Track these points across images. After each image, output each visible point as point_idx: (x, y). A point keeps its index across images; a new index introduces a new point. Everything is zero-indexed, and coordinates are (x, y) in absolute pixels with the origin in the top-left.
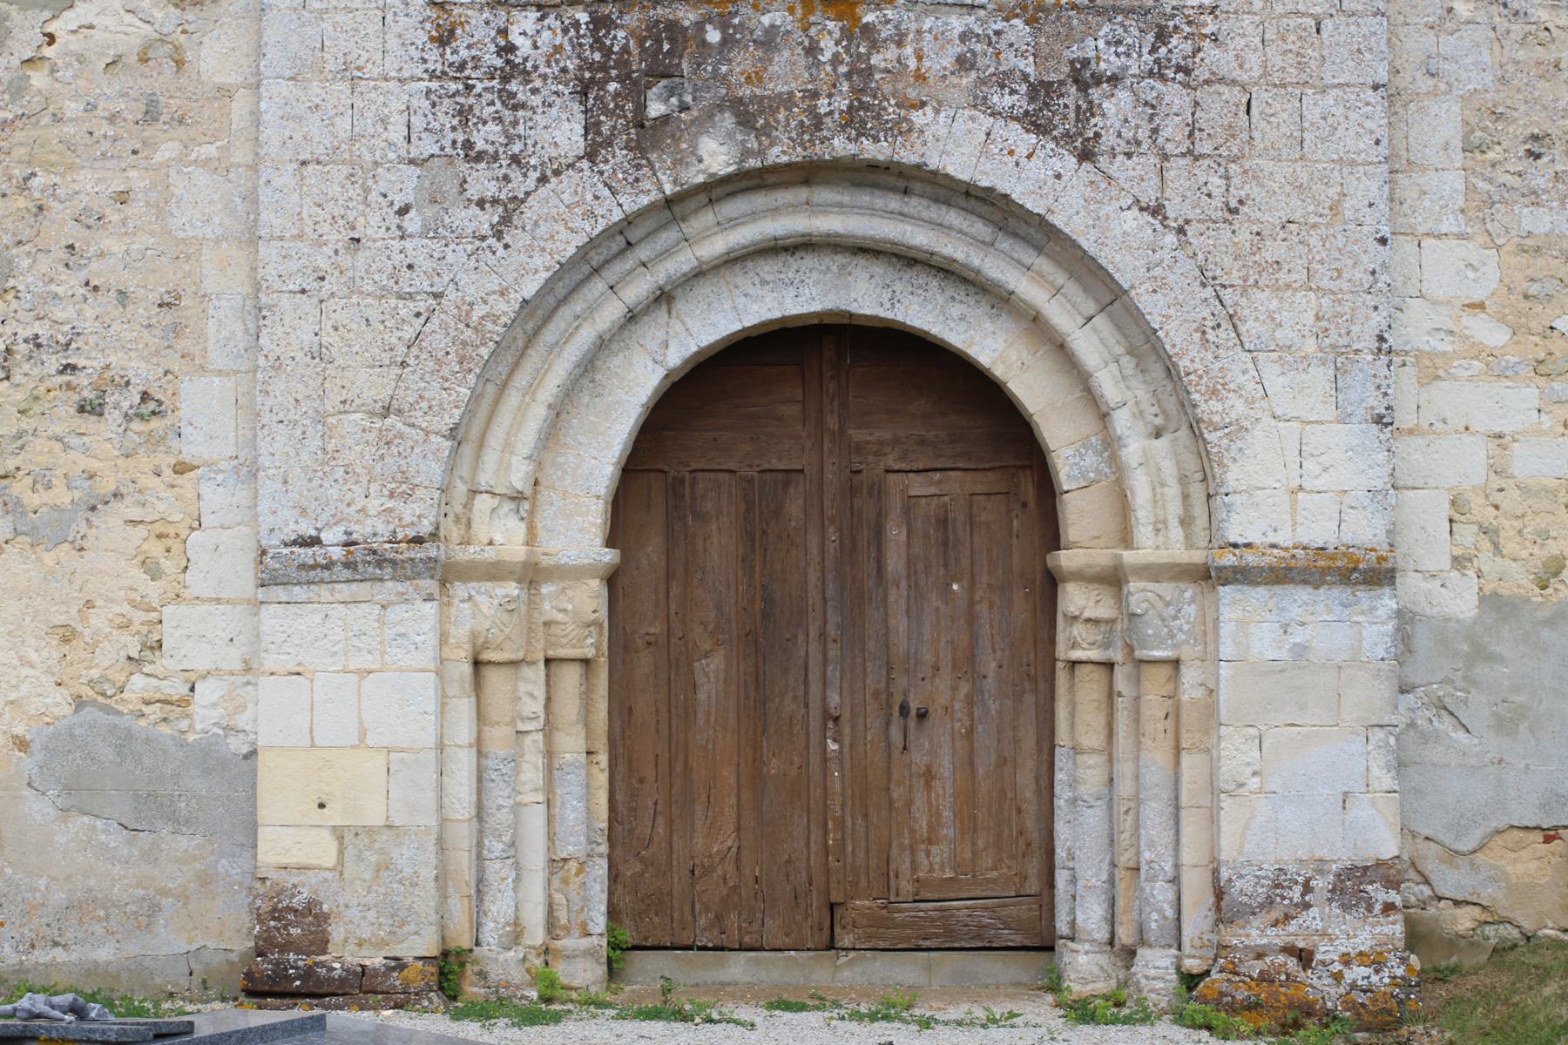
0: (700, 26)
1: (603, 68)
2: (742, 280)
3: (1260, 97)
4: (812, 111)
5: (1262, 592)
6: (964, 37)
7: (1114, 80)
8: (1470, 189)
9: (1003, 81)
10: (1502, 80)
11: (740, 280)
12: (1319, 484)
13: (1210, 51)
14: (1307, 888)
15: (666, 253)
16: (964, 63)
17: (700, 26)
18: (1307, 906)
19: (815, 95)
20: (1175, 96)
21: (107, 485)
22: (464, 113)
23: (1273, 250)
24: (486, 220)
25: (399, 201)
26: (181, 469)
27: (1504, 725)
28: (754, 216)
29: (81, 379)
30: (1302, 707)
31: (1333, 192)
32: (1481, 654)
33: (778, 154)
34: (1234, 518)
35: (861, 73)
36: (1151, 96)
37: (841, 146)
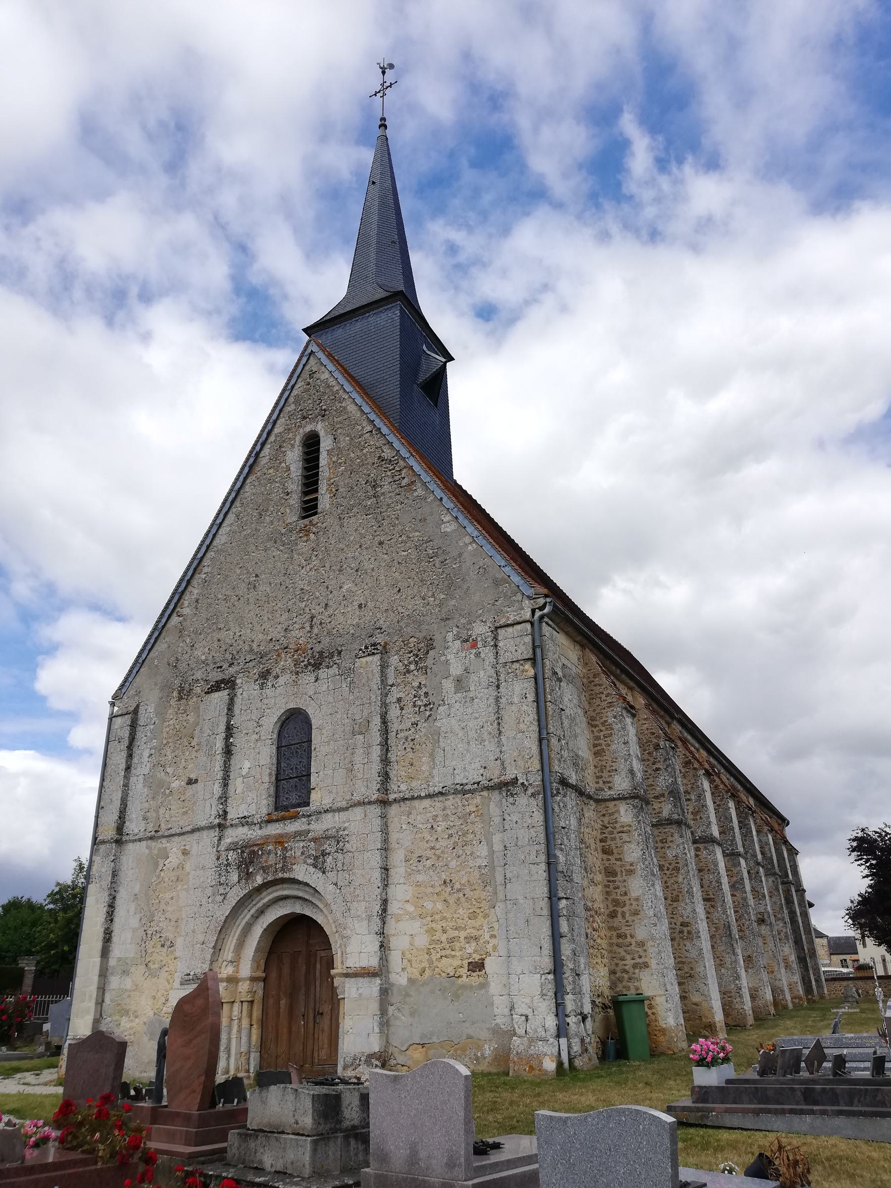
0: (258, 851)
1: (242, 862)
2: (276, 906)
3: (356, 854)
4: (275, 868)
5: (353, 979)
6: (303, 847)
7: (329, 854)
8: (406, 871)
9: (309, 856)
10: (412, 843)
11: (276, 907)
12: (364, 951)
13: (347, 845)
14: (360, 1061)
15: (258, 902)
16: (303, 853)
17: (258, 851)
18: (360, 1065)
19: (276, 864)
20: (340, 856)
21: (164, 963)
22: (220, 874)
23: (358, 892)
24: (220, 898)
25: (208, 895)
26: (175, 958)
27: (412, 1014)
28: (274, 892)
29: (162, 939)
30: (360, 1010)
31: (369, 876)
32: (407, 995)
33: (270, 878)
34: (348, 960)
35: (285, 858)
36: (335, 857)
37: (280, 875)
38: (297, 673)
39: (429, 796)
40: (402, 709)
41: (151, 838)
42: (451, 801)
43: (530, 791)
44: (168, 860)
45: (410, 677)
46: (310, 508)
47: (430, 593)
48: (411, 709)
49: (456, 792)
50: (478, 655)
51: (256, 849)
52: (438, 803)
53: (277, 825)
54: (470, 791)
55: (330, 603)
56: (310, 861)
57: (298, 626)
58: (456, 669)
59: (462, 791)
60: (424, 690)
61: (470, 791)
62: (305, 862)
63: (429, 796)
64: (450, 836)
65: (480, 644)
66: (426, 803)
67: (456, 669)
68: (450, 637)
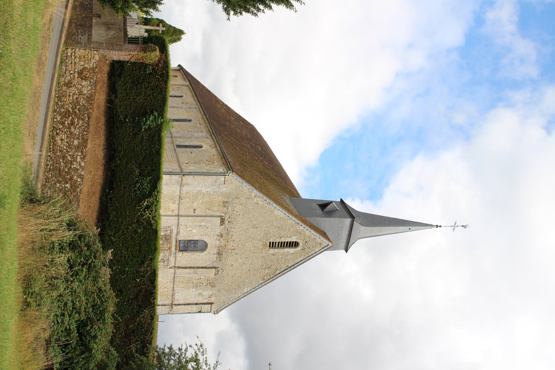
16: (165, 255)
20: (163, 267)
35: (165, 250)
38: (218, 247)
39: (173, 287)
40: (198, 279)
41: (180, 197)
42: (171, 292)
43: (169, 312)
44: (172, 204)
45: (206, 281)
46: (272, 245)
47: (228, 285)
48: (197, 282)
49: (173, 294)
50: (206, 298)
51: (169, 241)
52: (171, 289)
53: (175, 243)
54: (172, 297)
55: (237, 255)
56: (163, 258)
57: (233, 245)
58: (204, 293)
59: (173, 295)
60: (201, 285)
61: (172, 297)
62: (163, 256)
63: (173, 287)
64: (163, 292)
65: (209, 299)
66: (172, 286)
67: (204, 293)
68: (214, 291)
